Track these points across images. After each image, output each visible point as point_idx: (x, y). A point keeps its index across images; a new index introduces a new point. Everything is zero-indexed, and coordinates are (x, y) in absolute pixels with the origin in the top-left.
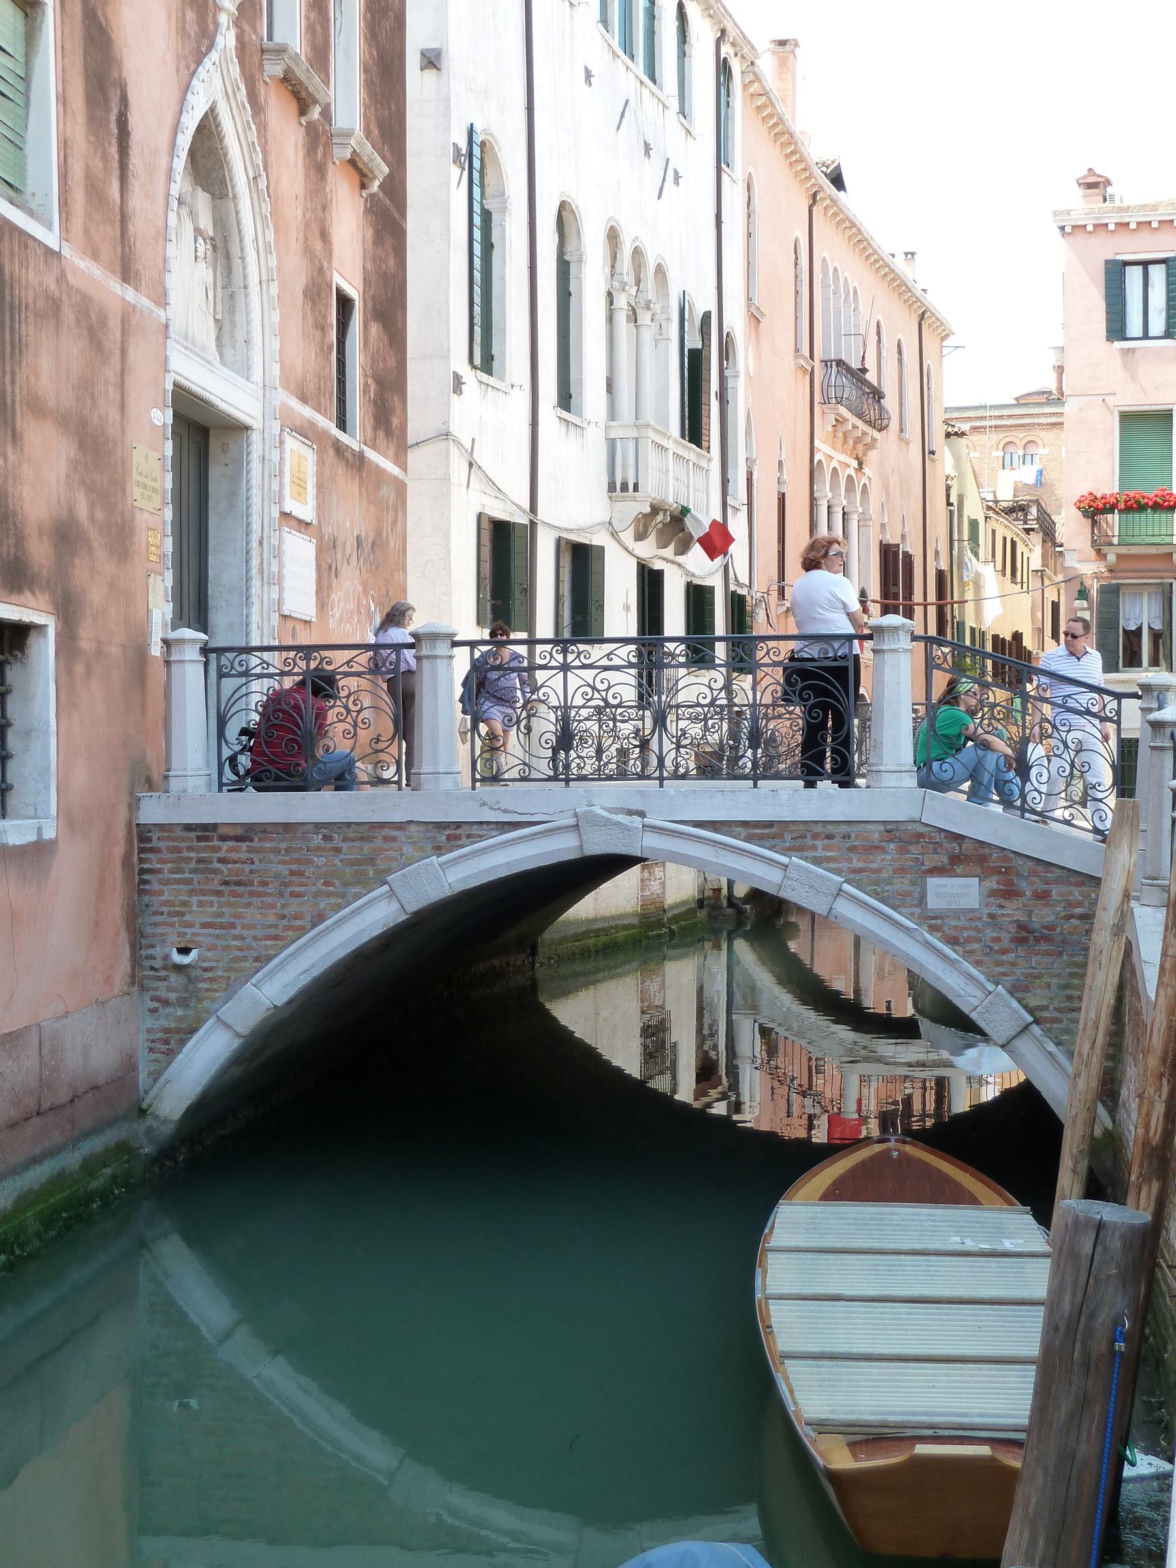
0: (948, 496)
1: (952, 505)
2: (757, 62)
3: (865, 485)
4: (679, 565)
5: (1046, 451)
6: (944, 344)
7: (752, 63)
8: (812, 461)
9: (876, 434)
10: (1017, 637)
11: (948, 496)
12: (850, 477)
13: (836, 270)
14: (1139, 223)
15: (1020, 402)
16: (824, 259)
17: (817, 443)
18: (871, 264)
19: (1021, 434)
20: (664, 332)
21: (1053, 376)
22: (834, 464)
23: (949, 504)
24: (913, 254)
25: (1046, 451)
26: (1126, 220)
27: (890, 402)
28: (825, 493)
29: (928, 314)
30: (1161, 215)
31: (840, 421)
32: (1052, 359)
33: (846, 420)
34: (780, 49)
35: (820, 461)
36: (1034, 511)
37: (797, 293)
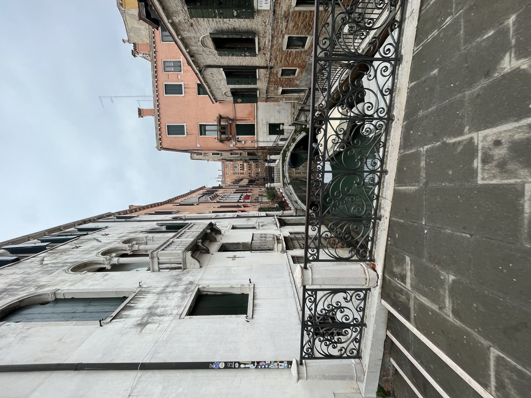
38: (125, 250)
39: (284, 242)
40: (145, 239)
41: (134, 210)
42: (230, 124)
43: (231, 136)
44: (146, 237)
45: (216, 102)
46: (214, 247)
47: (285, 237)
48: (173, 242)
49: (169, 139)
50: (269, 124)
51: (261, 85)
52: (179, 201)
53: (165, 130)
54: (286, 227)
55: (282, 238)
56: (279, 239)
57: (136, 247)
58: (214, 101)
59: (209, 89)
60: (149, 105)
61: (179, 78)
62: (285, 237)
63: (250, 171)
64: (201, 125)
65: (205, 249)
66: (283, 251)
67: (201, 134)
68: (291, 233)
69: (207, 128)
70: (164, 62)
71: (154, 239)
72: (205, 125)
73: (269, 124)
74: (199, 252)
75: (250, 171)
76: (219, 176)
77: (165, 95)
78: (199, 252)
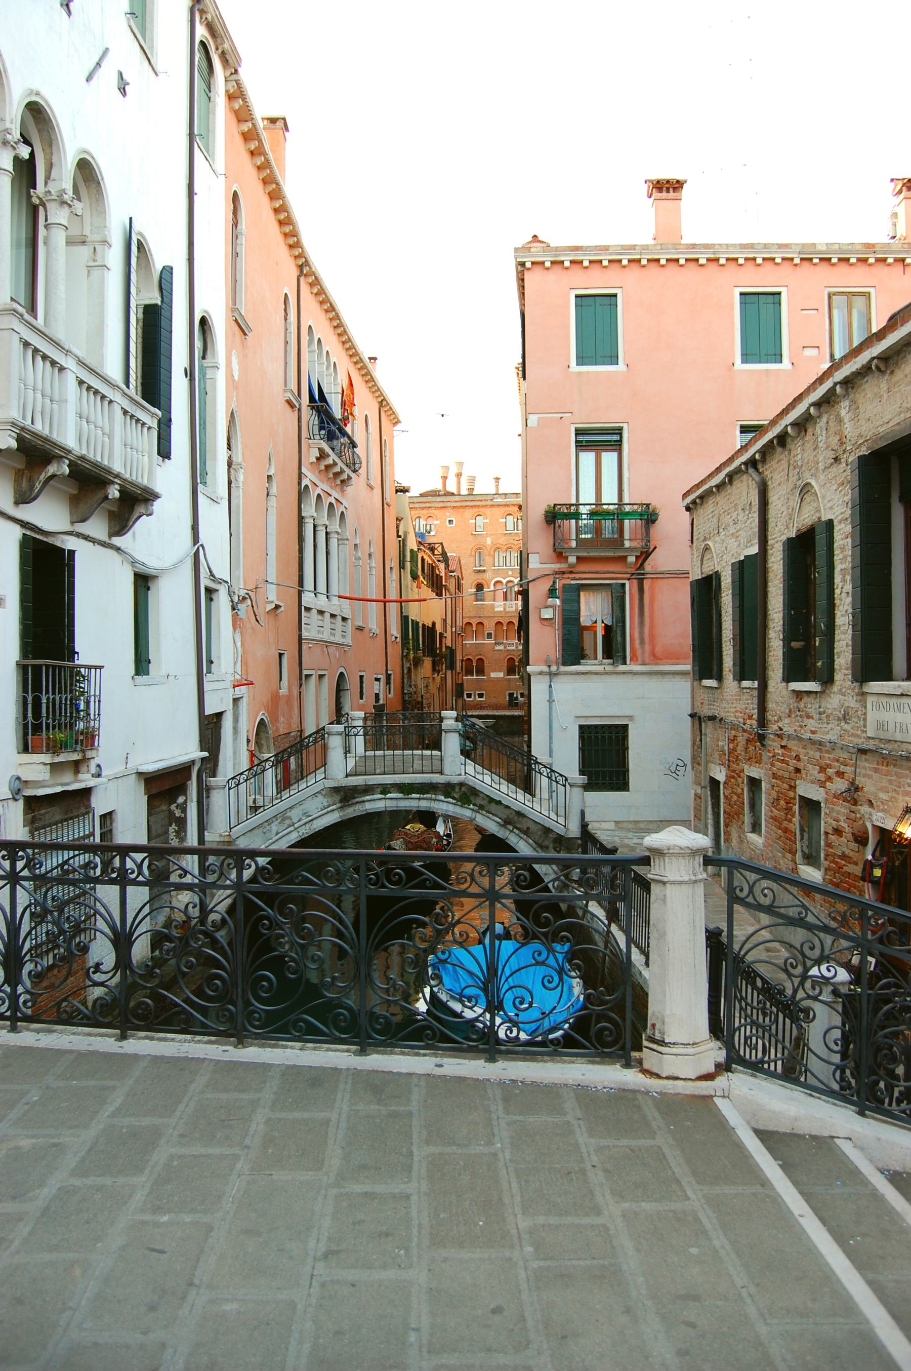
0: (398, 531)
1: (400, 537)
2: (240, 70)
3: (342, 512)
4: (118, 549)
5: (438, 522)
6: (395, 428)
7: (236, 71)
8: (300, 484)
9: (352, 475)
10: (434, 624)
11: (398, 531)
12: (331, 504)
13: (319, 340)
14: (591, 262)
15: (422, 495)
16: (310, 327)
17: (304, 470)
18: (347, 349)
19: (425, 512)
20: (99, 257)
21: (441, 481)
22: (318, 491)
23: (399, 536)
24: (375, 359)
25: (438, 522)
26: (580, 258)
27: (360, 451)
28: (309, 510)
29: (384, 403)
30: (611, 254)
31: (323, 455)
32: (440, 473)
33: (329, 456)
34: (272, 126)
35: (306, 486)
36: (440, 549)
37: (287, 343)
38: (48, 178)
39: (59, 789)
40: (97, 237)
41: (258, 141)
42: (624, 558)
43: (572, 559)
44: (105, 242)
45: (688, 509)
46: (49, 515)
47: (86, 793)
48: (62, 369)
49: (559, 295)
50: (625, 727)
51: (734, 698)
52: (313, 315)
53: (596, 283)
54: (145, 798)
55: (85, 780)
56: (77, 771)
57: (58, 215)
58: (689, 500)
59: (718, 487)
60: (703, 221)
61: (809, 352)
62: (86, 793)
63: (490, 627)
64: (619, 431)
65: (32, 487)
66: (18, 786)
67: (579, 432)
68: (107, 818)
69: (609, 459)
70: (867, 295)
71: (96, 273)
72: (617, 446)
73: (625, 727)
74: (21, 466)
75: (490, 627)
76: (472, 480)
77: (737, 291)
78: (21, 466)
